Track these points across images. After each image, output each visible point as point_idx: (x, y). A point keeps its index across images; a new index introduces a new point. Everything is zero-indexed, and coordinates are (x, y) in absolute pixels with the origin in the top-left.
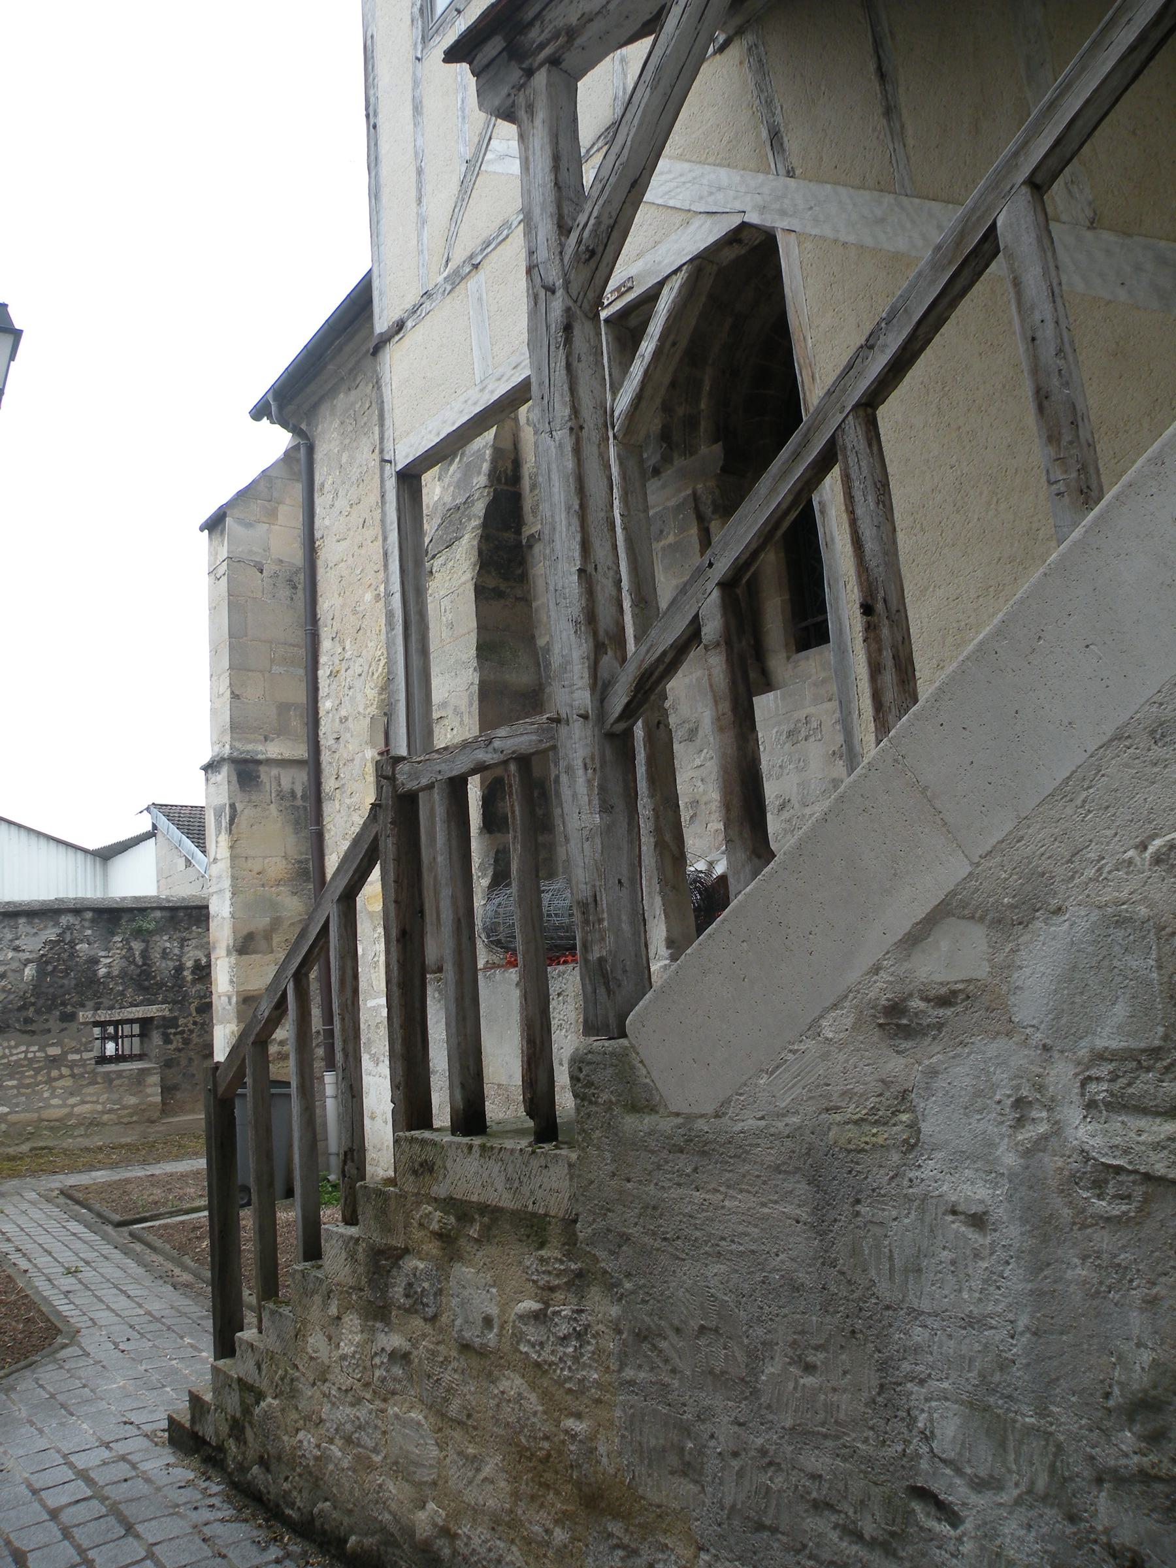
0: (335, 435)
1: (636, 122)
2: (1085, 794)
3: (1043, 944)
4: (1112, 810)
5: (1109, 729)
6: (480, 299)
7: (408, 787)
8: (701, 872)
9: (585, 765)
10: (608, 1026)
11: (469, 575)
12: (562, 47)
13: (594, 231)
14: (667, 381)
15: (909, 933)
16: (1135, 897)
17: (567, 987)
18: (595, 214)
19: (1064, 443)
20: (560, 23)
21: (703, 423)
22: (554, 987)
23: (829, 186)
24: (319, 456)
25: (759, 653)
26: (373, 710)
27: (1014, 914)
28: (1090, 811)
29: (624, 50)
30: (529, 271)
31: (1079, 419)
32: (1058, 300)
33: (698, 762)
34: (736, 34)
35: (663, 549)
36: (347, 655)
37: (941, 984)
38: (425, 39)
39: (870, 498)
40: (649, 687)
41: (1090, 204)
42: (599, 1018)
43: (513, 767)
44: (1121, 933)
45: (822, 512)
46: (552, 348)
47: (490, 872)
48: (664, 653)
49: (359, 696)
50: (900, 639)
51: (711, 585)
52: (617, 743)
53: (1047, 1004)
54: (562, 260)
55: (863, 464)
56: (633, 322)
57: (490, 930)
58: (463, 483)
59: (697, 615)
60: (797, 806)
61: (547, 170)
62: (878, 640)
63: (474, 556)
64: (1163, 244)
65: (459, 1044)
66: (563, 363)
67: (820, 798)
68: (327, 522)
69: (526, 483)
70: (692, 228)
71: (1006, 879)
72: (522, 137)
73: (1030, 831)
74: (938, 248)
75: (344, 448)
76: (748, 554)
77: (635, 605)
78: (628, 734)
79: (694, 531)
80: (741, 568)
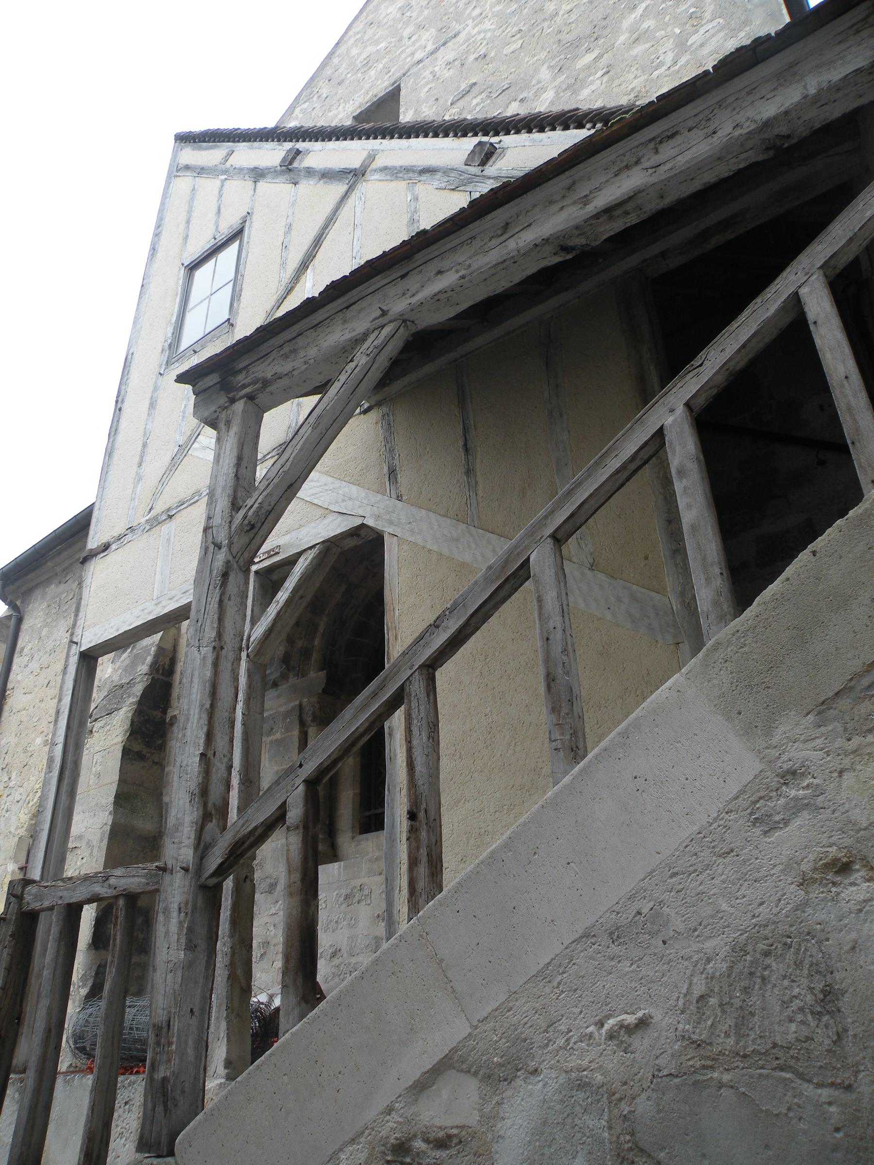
0: (41, 614)
1: (298, 447)
2: (559, 978)
3: (522, 1100)
4: (579, 992)
5: (580, 929)
6: (169, 540)
7: (32, 906)
8: (262, 1003)
9: (180, 909)
10: (159, 1143)
11: (120, 739)
12: (258, 390)
13: (257, 513)
14: (292, 622)
15: (418, 1081)
16: (594, 1065)
17: (132, 1092)
18: (259, 501)
19: (562, 714)
20: (259, 375)
21: (314, 654)
22: (121, 1096)
23: (423, 512)
24: (25, 626)
25: (331, 832)
26: (22, 832)
27: (501, 1073)
28: (563, 992)
29: (301, 399)
30: (205, 530)
31: (574, 698)
32: (566, 615)
33: (273, 911)
34: (376, 405)
35: (271, 742)
36: (11, 784)
37: (440, 1128)
38: (168, 363)
39: (423, 733)
40: (242, 852)
41: (591, 554)
42: (153, 1136)
43: (121, 902)
44: (581, 1095)
45: (390, 735)
46: (211, 587)
47: (90, 983)
48: (256, 828)
49: (14, 818)
50: (434, 841)
51: (299, 781)
52: (209, 894)
53: (523, 1153)
54: (230, 527)
55: (422, 708)
56: (275, 577)
57: (78, 1037)
58: (130, 668)
59: (285, 802)
60: (345, 955)
61: (232, 465)
62: (418, 840)
63: (127, 725)
64: (635, 587)
65: (21, 1154)
66: (217, 599)
67: (364, 951)
68: (19, 678)
69: (177, 677)
70: (327, 521)
71: (497, 1042)
72: (219, 440)
73: (517, 1004)
74: (490, 568)
75: (46, 625)
76: (329, 762)
77: (242, 783)
78: (218, 887)
79: (296, 732)
80: (322, 772)
